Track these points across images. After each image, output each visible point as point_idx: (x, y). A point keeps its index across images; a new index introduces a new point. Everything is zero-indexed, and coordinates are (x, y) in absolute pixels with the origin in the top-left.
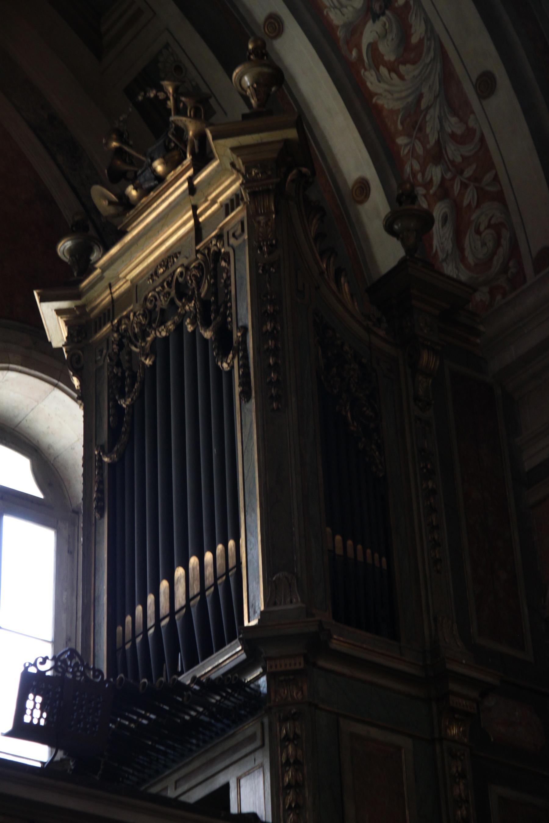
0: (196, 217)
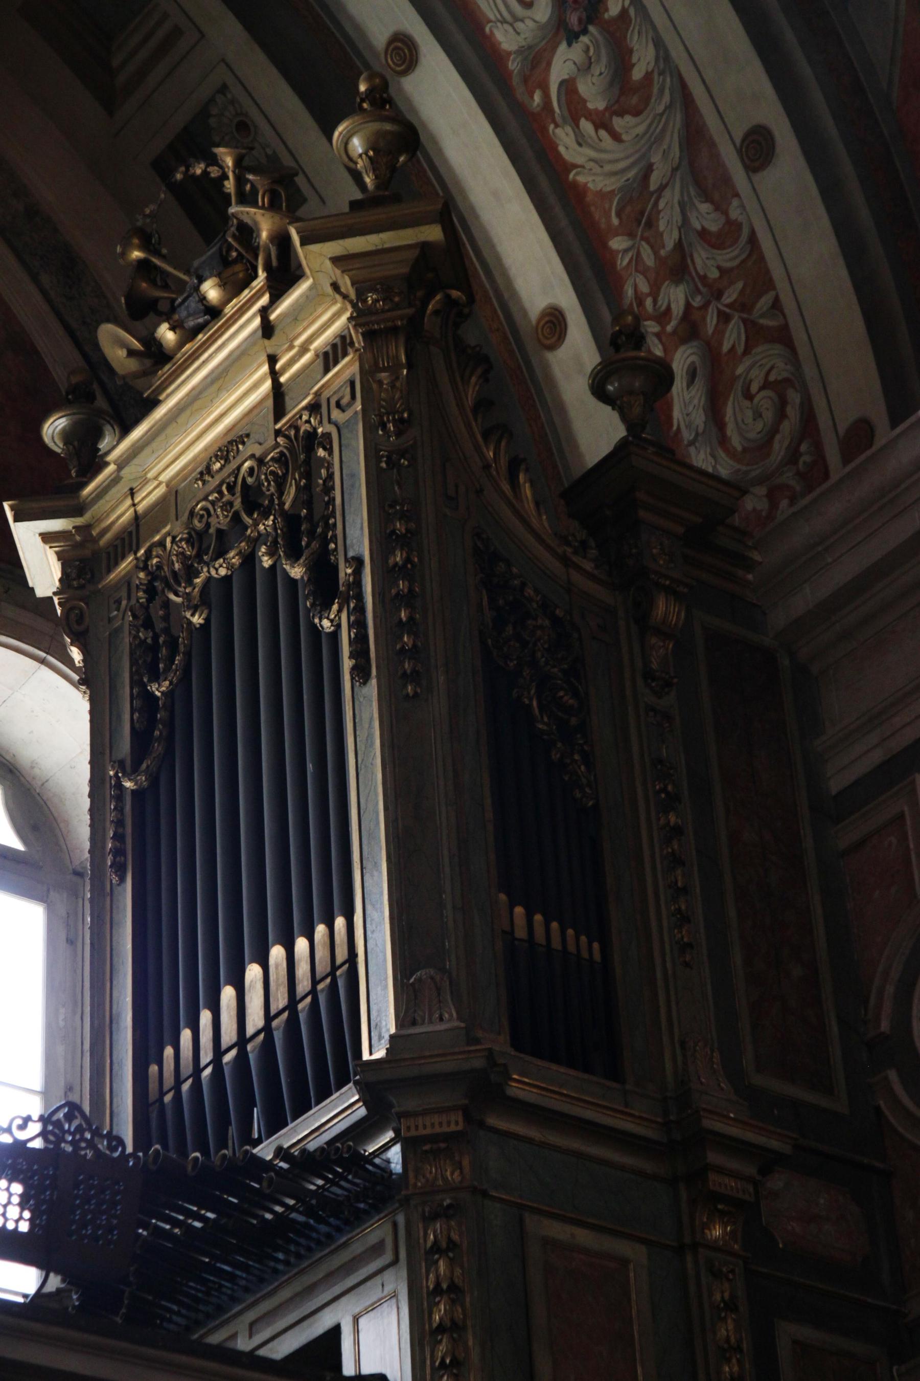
0: (274, 374)
